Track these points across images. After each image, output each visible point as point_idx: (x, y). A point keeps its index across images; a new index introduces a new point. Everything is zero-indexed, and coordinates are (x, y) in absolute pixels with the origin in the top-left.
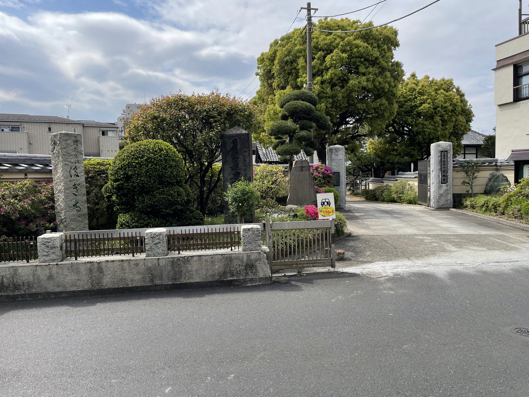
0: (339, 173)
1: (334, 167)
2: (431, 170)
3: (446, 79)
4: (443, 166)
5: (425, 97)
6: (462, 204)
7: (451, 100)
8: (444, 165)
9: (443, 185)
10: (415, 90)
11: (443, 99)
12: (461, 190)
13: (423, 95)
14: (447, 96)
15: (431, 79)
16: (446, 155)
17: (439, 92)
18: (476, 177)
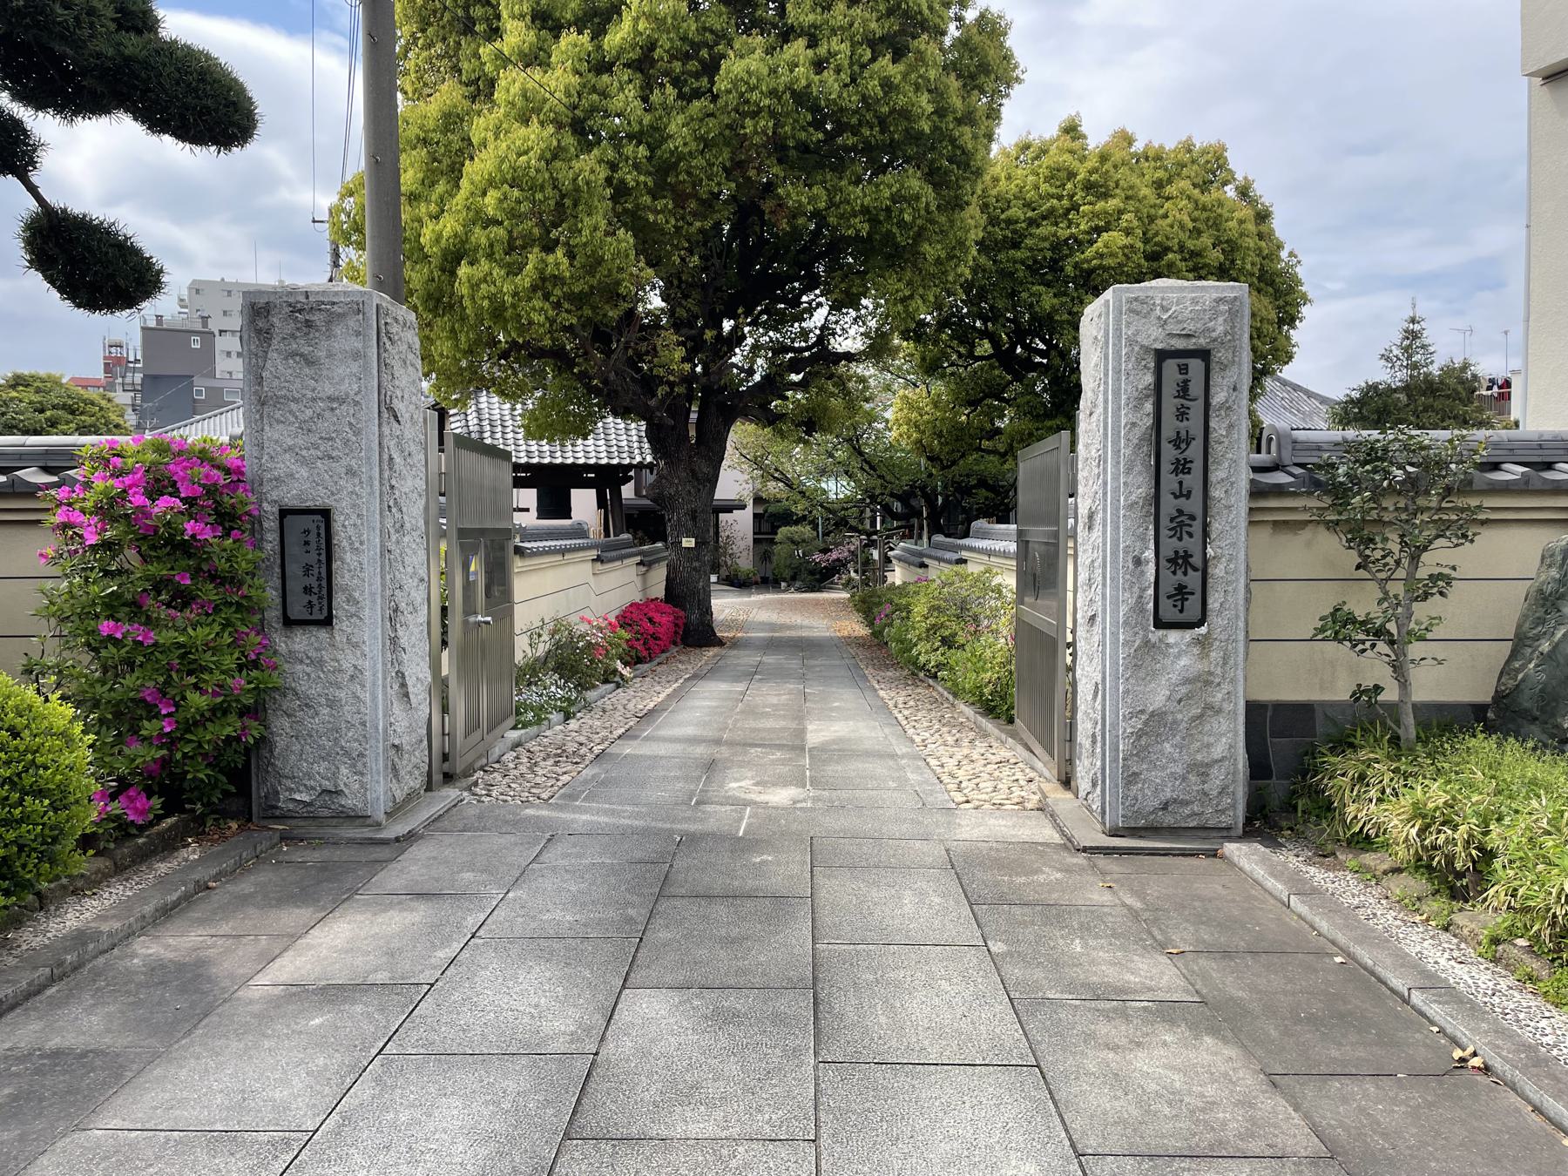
0: (326, 514)
1: (285, 465)
2: (1083, 511)
3: (1199, 143)
4: (1169, 481)
5: (1112, 204)
6: (1327, 808)
7: (1216, 224)
8: (1182, 467)
9: (1173, 636)
10: (1072, 175)
11: (1186, 219)
12: (1328, 677)
13: (1106, 196)
14: (1204, 209)
15: (1138, 147)
16: (1196, 388)
17: (1169, 190)
18: (1441, 582)
